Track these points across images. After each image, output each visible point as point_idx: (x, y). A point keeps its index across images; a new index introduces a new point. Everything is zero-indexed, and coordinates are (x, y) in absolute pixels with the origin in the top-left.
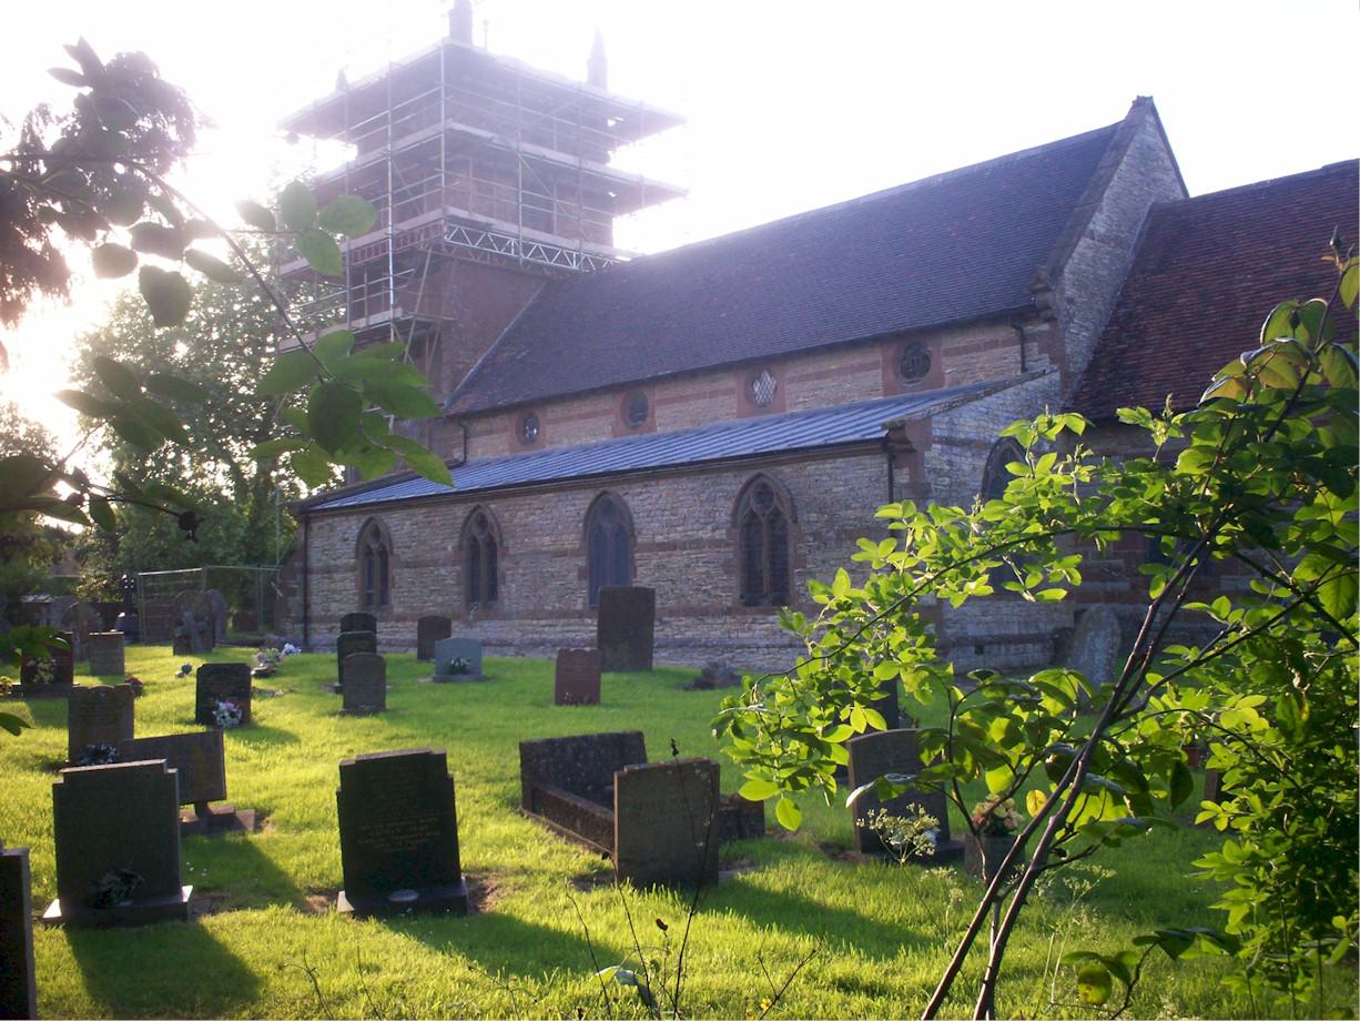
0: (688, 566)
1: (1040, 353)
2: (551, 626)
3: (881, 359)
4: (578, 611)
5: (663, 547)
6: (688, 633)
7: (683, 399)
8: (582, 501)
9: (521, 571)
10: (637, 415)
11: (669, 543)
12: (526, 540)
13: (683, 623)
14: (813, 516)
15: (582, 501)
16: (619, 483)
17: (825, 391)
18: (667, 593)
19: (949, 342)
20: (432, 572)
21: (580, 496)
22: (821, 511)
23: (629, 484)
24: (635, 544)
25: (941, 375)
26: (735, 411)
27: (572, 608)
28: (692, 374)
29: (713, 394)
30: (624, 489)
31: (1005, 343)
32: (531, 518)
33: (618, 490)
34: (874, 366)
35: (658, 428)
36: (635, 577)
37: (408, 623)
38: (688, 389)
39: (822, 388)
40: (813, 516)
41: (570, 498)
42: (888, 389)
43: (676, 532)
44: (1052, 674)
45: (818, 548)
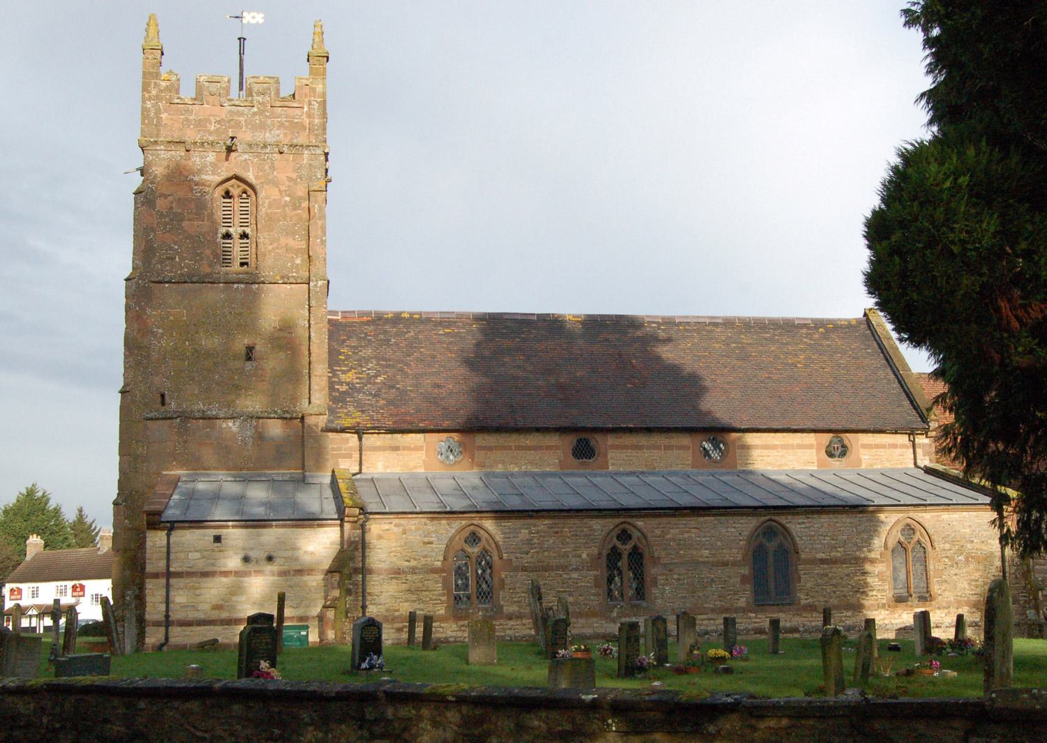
0: (848, 575)
1: (924, 455)
2: (710, 619)
3: (815, 443)
4: (741, 608)
5: (823, 561)
6: (847, 622)
7: (638, 447)
8: (747, 525)
9: (675, 577)
10: (838, 451)
11: (831, 559)
12: (682, 552)
13: (844, 614)
14: (947, 546)
15: (747, 525)
16: (783, 514)
17: (770, 458)
18: (829, 594)
19: (611, 440)
20: (561, 575)
21: (742, 521)
22: (953, 542)
23: (793, 515)
24: (799, 559)
25: (860, 460)
26: (690, 462)
27: (735, 605)
28: (649, 430)
29: (667, 448)
30: (786, 519)
31: (903, 446)
32: (686, 535)
33: (782, 519)
34: (810, 447)
35: (611, 467)
36: (800, 582)
37: (525, 621)
38: (642, 440)
39: (769, 456)
40: (947, 546)
41: (731, 522)
42: (562, 465)
43: (837, 551)
44: (267, 579)
45: (952, 566)
